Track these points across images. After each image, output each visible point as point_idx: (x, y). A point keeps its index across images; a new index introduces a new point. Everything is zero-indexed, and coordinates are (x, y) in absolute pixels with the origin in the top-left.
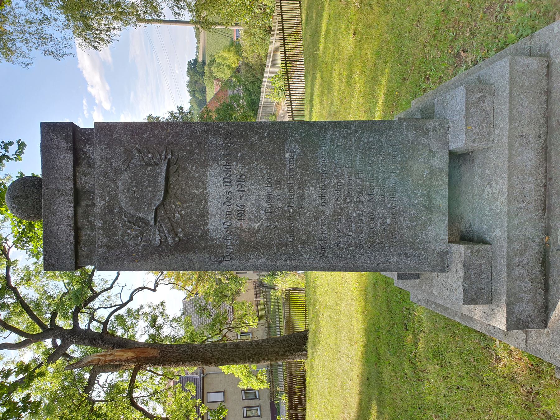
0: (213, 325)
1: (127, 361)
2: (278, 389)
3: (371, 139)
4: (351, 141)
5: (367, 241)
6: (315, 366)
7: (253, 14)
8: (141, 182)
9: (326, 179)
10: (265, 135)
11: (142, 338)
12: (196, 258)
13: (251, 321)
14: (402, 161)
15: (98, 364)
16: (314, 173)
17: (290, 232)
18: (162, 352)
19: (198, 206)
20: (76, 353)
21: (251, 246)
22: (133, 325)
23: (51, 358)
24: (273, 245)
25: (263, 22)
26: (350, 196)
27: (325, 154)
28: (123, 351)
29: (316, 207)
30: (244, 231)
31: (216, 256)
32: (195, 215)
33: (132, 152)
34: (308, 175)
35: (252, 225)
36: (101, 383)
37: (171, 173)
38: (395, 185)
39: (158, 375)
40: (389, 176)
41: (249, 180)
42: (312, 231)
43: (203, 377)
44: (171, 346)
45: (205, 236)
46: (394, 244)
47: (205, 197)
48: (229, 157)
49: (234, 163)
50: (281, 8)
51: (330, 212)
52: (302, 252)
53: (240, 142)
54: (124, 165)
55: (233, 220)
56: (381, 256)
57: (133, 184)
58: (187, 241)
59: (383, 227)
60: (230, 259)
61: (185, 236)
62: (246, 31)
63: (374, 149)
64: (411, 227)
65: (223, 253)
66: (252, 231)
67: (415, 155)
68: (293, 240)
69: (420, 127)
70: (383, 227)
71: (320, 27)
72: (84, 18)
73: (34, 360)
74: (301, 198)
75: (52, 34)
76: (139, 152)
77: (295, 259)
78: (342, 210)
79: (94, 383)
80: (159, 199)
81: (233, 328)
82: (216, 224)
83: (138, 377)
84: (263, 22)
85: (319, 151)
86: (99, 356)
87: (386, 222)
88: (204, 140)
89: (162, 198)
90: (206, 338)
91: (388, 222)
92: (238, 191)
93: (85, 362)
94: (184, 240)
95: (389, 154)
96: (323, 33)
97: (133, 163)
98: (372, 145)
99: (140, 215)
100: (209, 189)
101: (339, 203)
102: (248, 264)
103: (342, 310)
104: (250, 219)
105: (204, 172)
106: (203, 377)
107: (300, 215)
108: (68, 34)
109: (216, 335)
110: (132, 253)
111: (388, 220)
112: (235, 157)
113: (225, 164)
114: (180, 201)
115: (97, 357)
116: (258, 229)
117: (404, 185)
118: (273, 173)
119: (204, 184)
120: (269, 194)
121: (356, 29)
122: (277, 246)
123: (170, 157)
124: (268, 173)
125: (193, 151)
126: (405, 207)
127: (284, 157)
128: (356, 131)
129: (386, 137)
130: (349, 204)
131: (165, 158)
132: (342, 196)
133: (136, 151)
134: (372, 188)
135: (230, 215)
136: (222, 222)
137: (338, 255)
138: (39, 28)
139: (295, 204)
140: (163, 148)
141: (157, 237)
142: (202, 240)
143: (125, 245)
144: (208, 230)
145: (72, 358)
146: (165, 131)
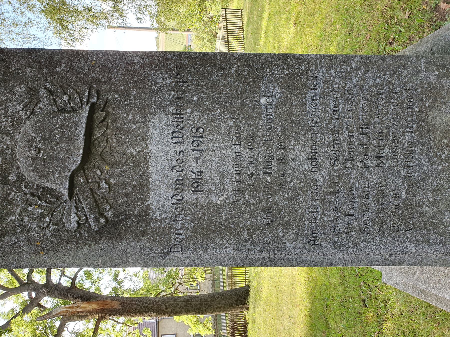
0: (167, 280)
1: (92, 312)
2: (221, 333)
3: (378, 81)
4: (351, 82)
5: (375, 222)
6: (256, 320)
7: (202, 22)
8: (50, 136)
9: (318, 135)
10: (233, 71)
11: (106, 292)
12: (130, 248)
13: (199, 276)
14: (421, 112)
15: (66, 315)
16: (300, 126)
17: (267, 209)
18: (122, 304)
19: (134, 172)
20: (49, 303)
21: (211, 230)
22: (99, 279)
23: (26, 309)
24: (242, 228)
25: (210, 29)
26: (351, 159)
27: (316, 100)
28: (88, 303)
29: (304, 174)
30: (202, 208)
31: (160, 245)
32: (130, 185)
33: (39, 92)
34: (293, 129)
35: (213, 199)
36: (70, 330)
37: (96, 124)
38: (412, 144)
39: (119, 323)
40: (404, 132)
41: (209, 134)
42: (299, 208)
43: (158, 322)
44: (131, 299)
45: (144, 215)
46: (412, 226)
47: (145, 159)
48: (180, 102)
49: (188, 110)
50: (226, 15)
51: (324, 182)
52: (284, 239)
53: (197, 81)
54: (26, 111)
55: (186, 193)
56: (393, 244)
57: (39, 139)
58: (117, 223)
59: (396, 203)
60: (180, 250)
61: (115, 216)
62: (197, 36)
63: (382, 94)
64: (434, 204)
65: (170, 240)
66: (213, 209)
67: (438, 103)
68: (272, 221)
69: (444, 65)
70: (396, 203)
71: (261, 26)
72: (61, 21)
73: (13, 310)
74: (282, 161)
75: (35, 34)
76: (50, 92)
77: (275, 249)
78: (340, 178)
79: (63, 331)
80: (75, 161)
81: (184, 282)
82: (160, 198)
83: (102, 325)
84: (210, 29)
85: (308, 95)
86: (67, 308)
87: (401, 196)
88: (145, 77)
89: (79, 159)
90: (161, 291)
91: (403, 196)
92: (194, 150)
93: (55, 313)
94: (112, 222)
95: (403, 101)
96: (264, 29)
97: (40, 108)
98: (379, 89)
99: (49, 185)
100: (151, 147)
101: (336, 168)
102: (207, 257)
103: (284, 273)
104: (210, 190)
105: (144, 123)
106: (158, 322)
107: (281, 185)
108: (49, 35)
109: (169, 288)
110: (35, 240)
111: (403, 193)
112: (188, 102)
113: (174, 112)
114: (109, 165)
115: (65, 309)
116: (221, 206)
117: (423, 145)
118: (243, 125)
119: (143, 140)
120: (237, 155)
121: (297, 19)
122: (248, 230)
123: (94, 100)
124: (237, 126)
125: (129, 93)
126: (425, 174)
127: (259, 102)
128: (358, 69)
129: (398, 78)
130: (350, 171)
131: (88, 101)
132: (341, 158)
133: (45, 91)
134: (381, 148)
135: (182, 184)
136: (169, 195)
137: (335, 242)
138: (24, 29)
139: (274, 169)
140: (85, 88)
141: (74, 218)
142: (139, 221)
143: (25, 230)
144: (149, 208)
145: (45, 308)
146: (88, 63)
